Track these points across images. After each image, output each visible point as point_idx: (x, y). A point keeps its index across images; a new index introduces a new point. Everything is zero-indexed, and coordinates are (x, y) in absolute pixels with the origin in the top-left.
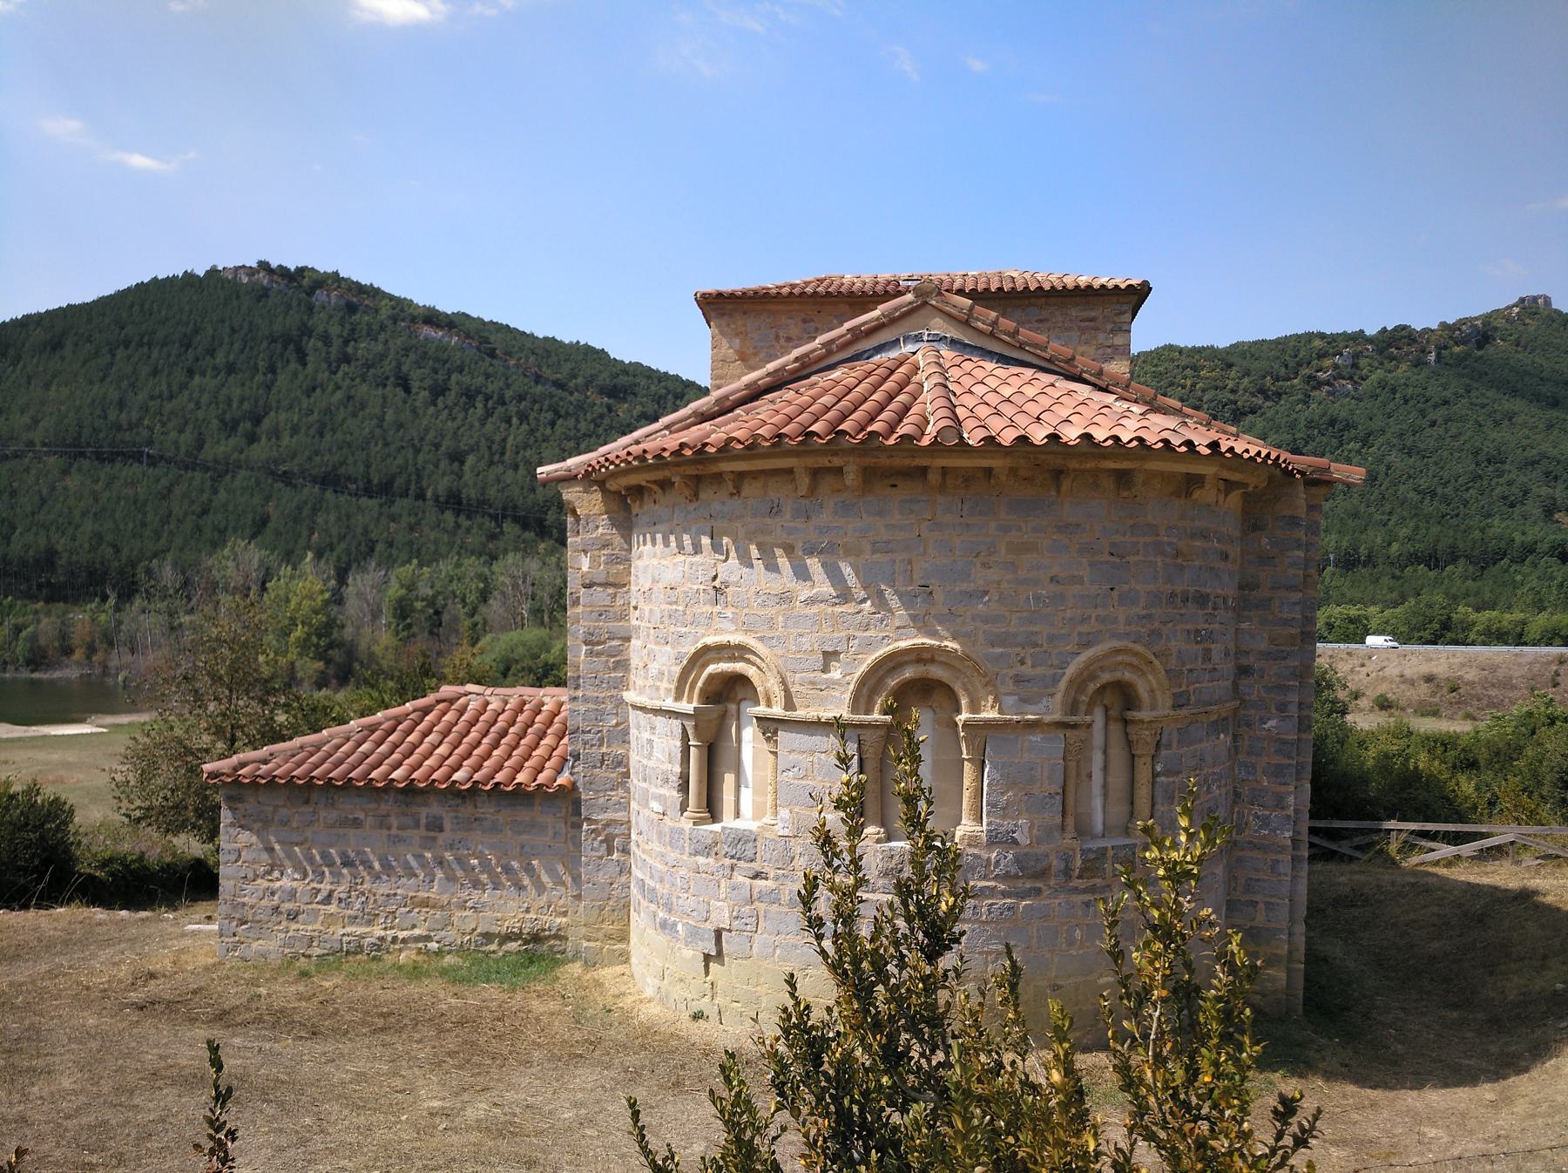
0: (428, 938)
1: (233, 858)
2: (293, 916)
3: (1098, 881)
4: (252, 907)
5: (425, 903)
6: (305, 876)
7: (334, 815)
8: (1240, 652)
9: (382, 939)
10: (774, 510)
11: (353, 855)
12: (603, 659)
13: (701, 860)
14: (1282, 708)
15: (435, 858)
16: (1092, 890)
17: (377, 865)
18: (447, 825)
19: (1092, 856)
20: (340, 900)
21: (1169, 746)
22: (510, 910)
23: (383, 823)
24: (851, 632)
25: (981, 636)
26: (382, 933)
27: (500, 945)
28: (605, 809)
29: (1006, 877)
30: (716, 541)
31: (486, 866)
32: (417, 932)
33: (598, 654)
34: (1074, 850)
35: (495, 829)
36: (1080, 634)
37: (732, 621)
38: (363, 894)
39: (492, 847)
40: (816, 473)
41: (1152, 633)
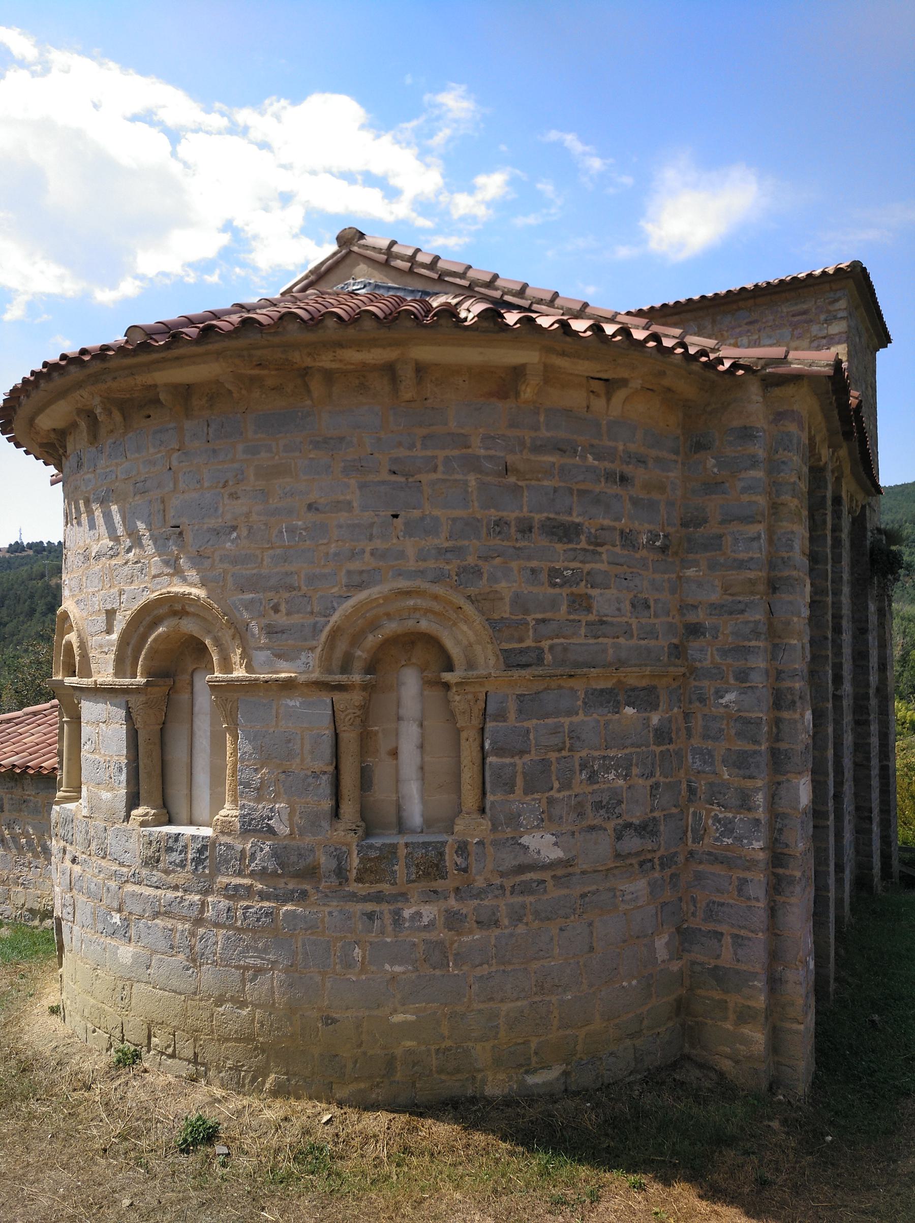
3: (385, 887)
8: (684, 608)
14: (742, 676)
16: (378, 898)
19: (373, 854)
21: (501, 716)
25: (230, 580)
27: (41, 921)
29: (262, 874)
34: (348, 845)
36: (349, 573)
41: (463, 571)
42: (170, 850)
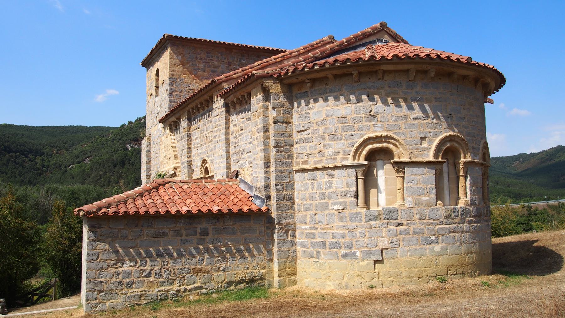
0: (201, 288)
1: (95, 258)
2: (130, 285)
4: (106, 283)
5: (200, 271)
6: (137, 263)
7: (152, 231)
9: (178, 291)
10: (399, 85)
11: (162, 251)
12: (283, 153)
13: (372, 223)
15: (204, 248)
17: (175, 255)
18: (210, 232)
20: (156, 274)
22: (239, 269)
23: (178, 234)
24: (430, 130)
26: (178, 288)
27: (235, 286)
28: (286, 218)
30: (370, 97)
31: (229, 251)
32: (196, 285)
33: (281, 152)
35: (233, 232)
37: (381, 127)
38: (168, 270)
39: (231, 241)
40: (418, 72)
42: (454, 212)
